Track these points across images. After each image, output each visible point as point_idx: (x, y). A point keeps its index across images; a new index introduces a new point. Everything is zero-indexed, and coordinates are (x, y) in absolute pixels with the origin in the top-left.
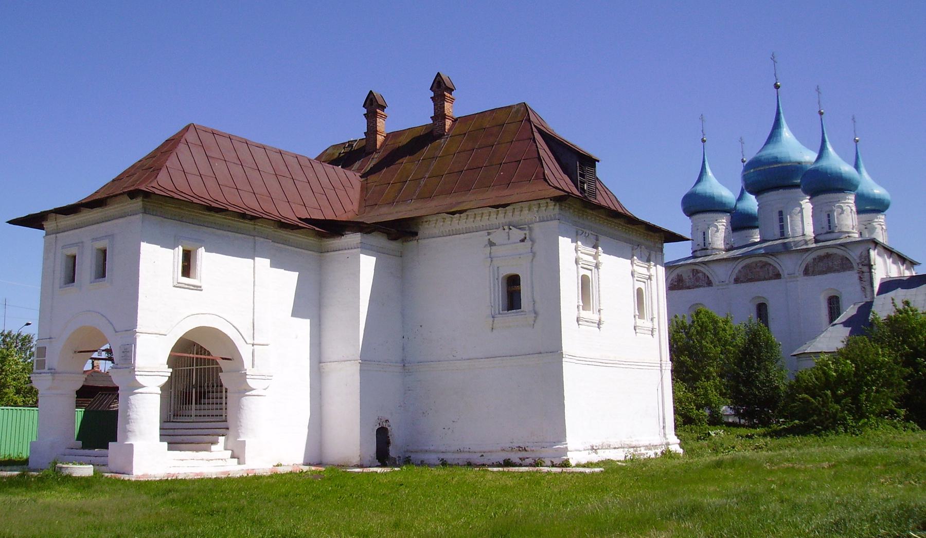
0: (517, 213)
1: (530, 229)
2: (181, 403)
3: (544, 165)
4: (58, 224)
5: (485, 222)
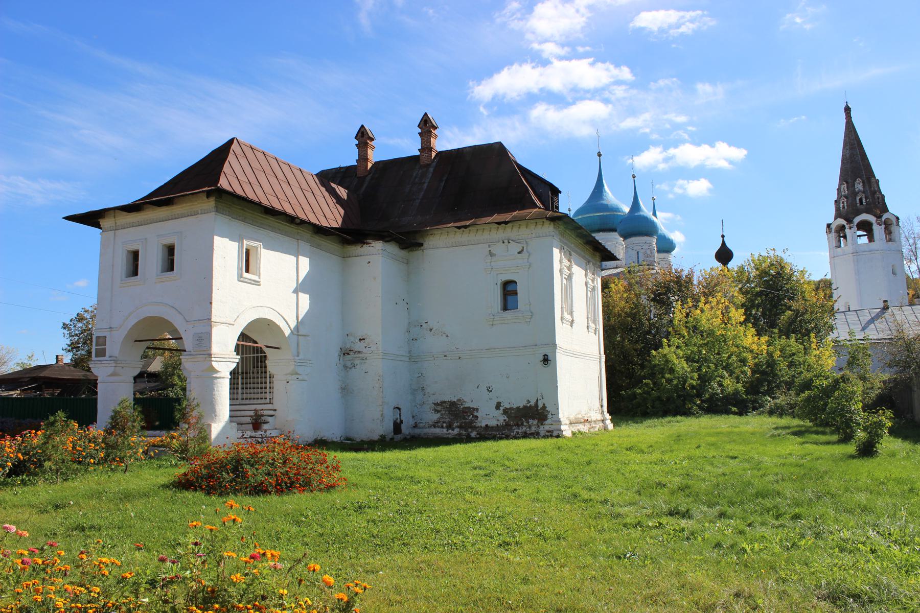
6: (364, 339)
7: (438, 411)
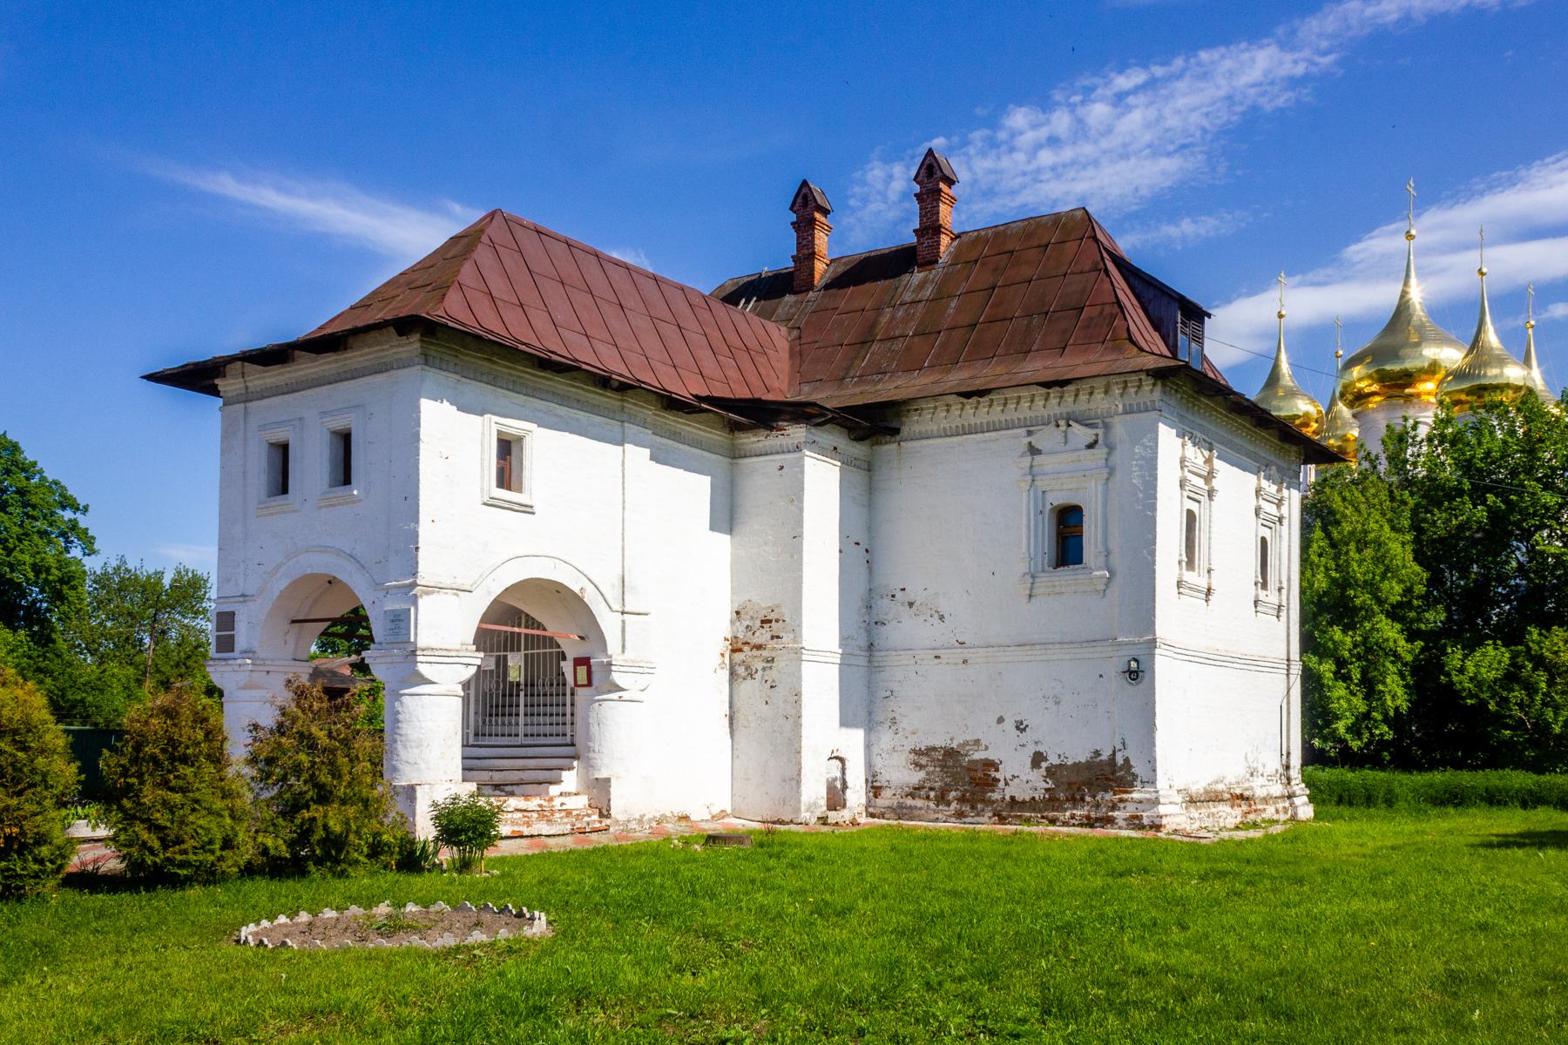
0: (1083, 397)
1: (1107, 427)
4: (249, 384)
5: (1025, 411)
7: (921, 767)
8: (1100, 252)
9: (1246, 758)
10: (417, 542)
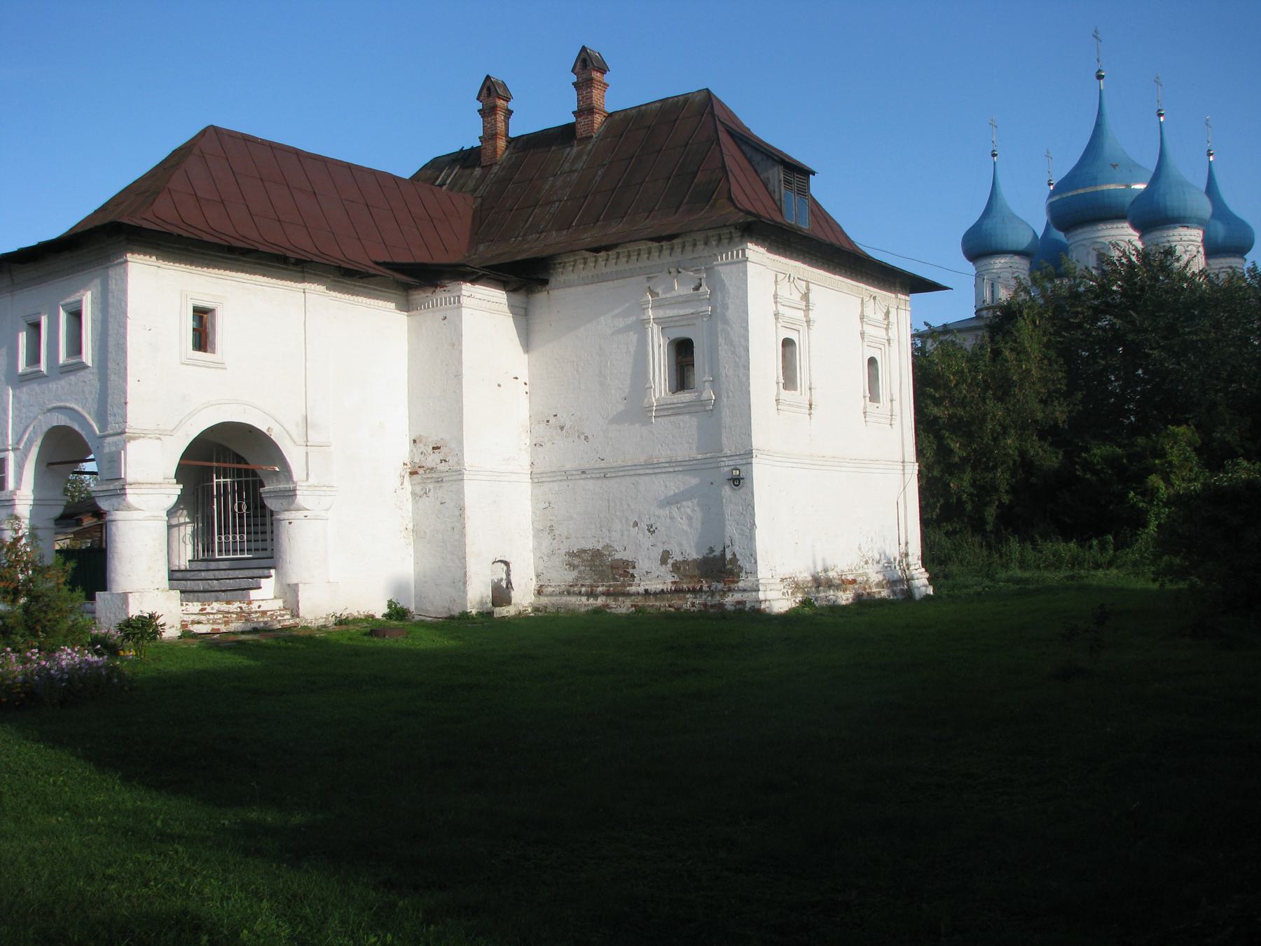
2: (234, 526)
3: (730, 177)
6: (438, 448)
8: (715, 125)
9: (860, 549)
10: (126, 398)
